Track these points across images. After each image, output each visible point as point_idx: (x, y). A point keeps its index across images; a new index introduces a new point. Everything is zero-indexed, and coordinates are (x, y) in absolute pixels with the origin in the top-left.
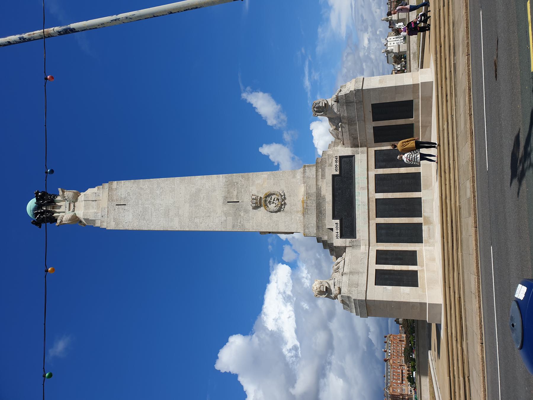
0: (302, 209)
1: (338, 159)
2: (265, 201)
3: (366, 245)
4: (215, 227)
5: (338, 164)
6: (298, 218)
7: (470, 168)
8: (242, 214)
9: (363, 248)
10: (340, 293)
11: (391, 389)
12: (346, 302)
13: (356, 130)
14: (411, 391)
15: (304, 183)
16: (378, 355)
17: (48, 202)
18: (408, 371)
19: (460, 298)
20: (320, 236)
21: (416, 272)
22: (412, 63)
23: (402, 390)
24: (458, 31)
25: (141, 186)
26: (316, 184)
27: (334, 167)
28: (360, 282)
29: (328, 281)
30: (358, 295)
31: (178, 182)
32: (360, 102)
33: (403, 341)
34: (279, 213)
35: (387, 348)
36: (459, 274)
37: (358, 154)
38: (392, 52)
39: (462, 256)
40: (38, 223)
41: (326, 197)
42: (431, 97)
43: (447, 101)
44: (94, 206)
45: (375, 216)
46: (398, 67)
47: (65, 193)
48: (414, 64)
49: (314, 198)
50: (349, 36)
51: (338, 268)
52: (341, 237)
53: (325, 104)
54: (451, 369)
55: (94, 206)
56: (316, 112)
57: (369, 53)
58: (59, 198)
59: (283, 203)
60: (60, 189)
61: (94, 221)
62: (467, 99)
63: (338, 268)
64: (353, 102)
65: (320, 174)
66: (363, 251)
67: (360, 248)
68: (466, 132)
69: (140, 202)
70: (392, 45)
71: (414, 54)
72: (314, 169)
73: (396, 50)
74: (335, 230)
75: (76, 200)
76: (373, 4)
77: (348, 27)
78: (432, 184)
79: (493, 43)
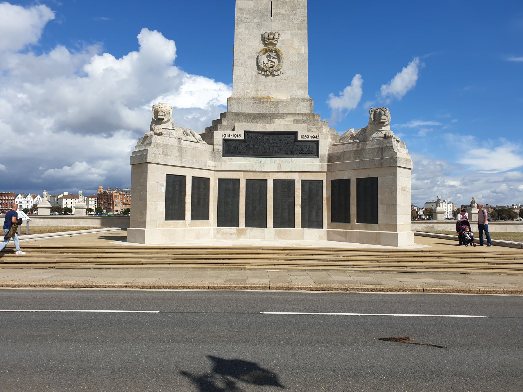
0: (260, 96)
1: (315, 139)
2: (271, 51)
5: (310, 139)
6: (249, 91)
7: (280, 285)
8: (256, 21)
9: (211, 164)
10: (156, 134)
11: (118, 194)
12: (145, 140)
13: (348, 159)
15: (291, 100)
19: (142, 264)
20: (228, 117)
23: (118, 204)
24: (456, 279)
28: (169, 157)
34: (256, 67)
37: (320, 162)
38: (437, 206)
39: (188, 269)
41: (272, 124)
42: (379, 244)
43: (371, 261)
45: (247, 178)
46: (421, 212)
48: (421, 227)
49: (272, 111)
50: (461, 167)
51: (187, 135)
52: (225, 141)
53: (384, 123)
54: (71, 249)
56: (375, 112)
57: (439, 186)
59: (268, 73)
62: (368, 286)
63: (187, 135)
64: (382, 156)
65: (301, 118)
66: (211, 165)
67: (212, 160)
68: (327, 282)
71: (433, 227)
73: (438, 210)
74: (231, 133)
77: (470, 166)
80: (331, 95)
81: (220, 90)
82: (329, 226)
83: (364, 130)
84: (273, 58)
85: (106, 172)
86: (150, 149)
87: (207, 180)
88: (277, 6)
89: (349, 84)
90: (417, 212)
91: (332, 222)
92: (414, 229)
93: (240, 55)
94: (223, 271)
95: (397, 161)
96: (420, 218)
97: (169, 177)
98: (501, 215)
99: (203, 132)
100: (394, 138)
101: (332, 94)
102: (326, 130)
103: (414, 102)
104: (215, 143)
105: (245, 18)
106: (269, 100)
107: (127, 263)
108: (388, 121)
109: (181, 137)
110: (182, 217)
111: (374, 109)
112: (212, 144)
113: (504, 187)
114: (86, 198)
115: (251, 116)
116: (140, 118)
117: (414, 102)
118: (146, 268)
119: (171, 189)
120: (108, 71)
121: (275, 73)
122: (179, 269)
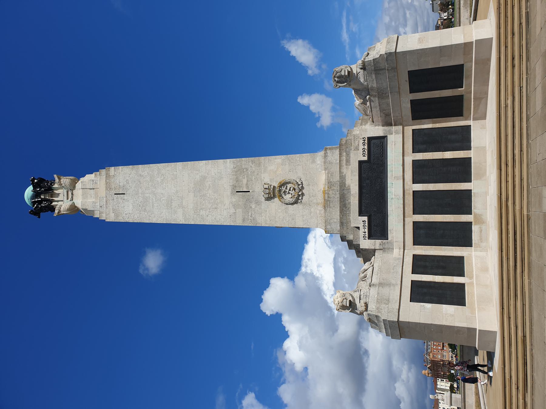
0: (323, 201)
1: (366, 142)
2: (280, 191)
3: (400, 249)
4: (223, 220)
5: (366, 147)
6: (318, 212)
8: (253, 206)
9: (397, 252)
10: (366, 310)
11: (431, 355)
12: (374, 321)
13: (388, 105)
14: (452, 357)
17: (45, 190)
19: (524, 336)
20: (345, 234)
21: (412, 91)
25: (140, 172)
26: (340, 171)
27: (361, 151)
28: (391, 297)
31: (180, 168)
36: (524, 305)
37: (392, 134)
39: (530, 283)
40: (36, 212)
41: (351, 188)
42: (489, 60)
43: (513, 66)
44: (92, 194)
46: (445, 15)
47: (62, 180)
48: (465, 14)
49: (337, 188)
52: (370, 237)
53: (349, 72)
55: (92, 194)
56: (338, 82)
58: (56, 186)
60: (55, 176)
61: (93, 211)
64: (384, 69)
65: (344, 158)
66: (399, 251)
67: (393, 251)
69: (140, 191)
72: (337, 152)
74: (362, 230)
75: (74, 187)
78: (485, 173)
80: (318, 125)
81: (315, 237)
82: (468, 118)
83: (356, 91)
84: (286, 189)
85: (405, 363)
86: (383, 318)
88: (240, 187)
89: (308, 107)
91: (462, 116)
92: (468, 21)
93: (284, 221)
94: (533, 241)
95: (390, 53)
97: (413, 299)
99: (361, 260)
100: (365, 59)
101: (317, 124)
102: (356, 131)
103: (325, 42)
105: (251, 216)
106: (327, 192)
107: (525, 355)
108: (346, 67)
109: (368, 283)
110: (462, 286)
111: (334, 84)
112: (374, 250)
114: (437, 391)
115: (343, 209)
116: (347, 323)
117: (325, 42)
118: (531, 333)
120: (301, 346)
121: (300, 186)
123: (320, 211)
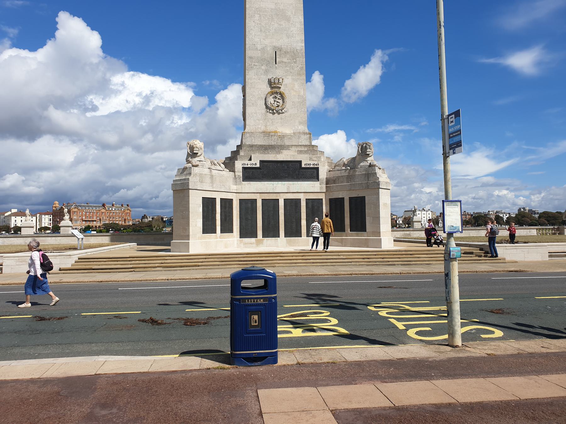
0: (269, 131)
2: (277, 93)
5: (312, 166)
6: (260, 126)
8: (263, 67)
9: (234, 188)
10: (193, 166)
11: (76, 210)
13: (342, 182)
15: (294, 133)
16: (104, 198)
18: (96, 227)
19: (199, 266)
20: (244, 148)
21: (351, 199)
22: (401, 232)
29: (203, 155)
30: (193, 182)
32: (368, 186)
33: (125, 222)
35: (117, 207)
38: (414, 215)
42: (368, 247)
43: (363, 259)
46: (400, 221)
48: (399, 234)
49: (280, 143)
51: (215, 164)
53: (369, 154)
56: (362, 146)
59: (275, 111)
62: (364, 272)
63: (215, 164)
64: (368, 180)
66: (231, 187)
70: (423, 216)
71: (409, 235)
73: (415, 219)
74: (249, 162)
76: (466, 197)
79: (405, 286)
87: (231, 201)
88: (280, 55)
90: (396, 221)
96: (399, 227)
98: (478, 221)
104: (236, 170)
112: (234, 171)
113: (482, 193)
114: (38, 215)
118: (202, 269)
119: (206, 209)
121: (280, 111)
122: (228, 268)
123: (260, 128)
